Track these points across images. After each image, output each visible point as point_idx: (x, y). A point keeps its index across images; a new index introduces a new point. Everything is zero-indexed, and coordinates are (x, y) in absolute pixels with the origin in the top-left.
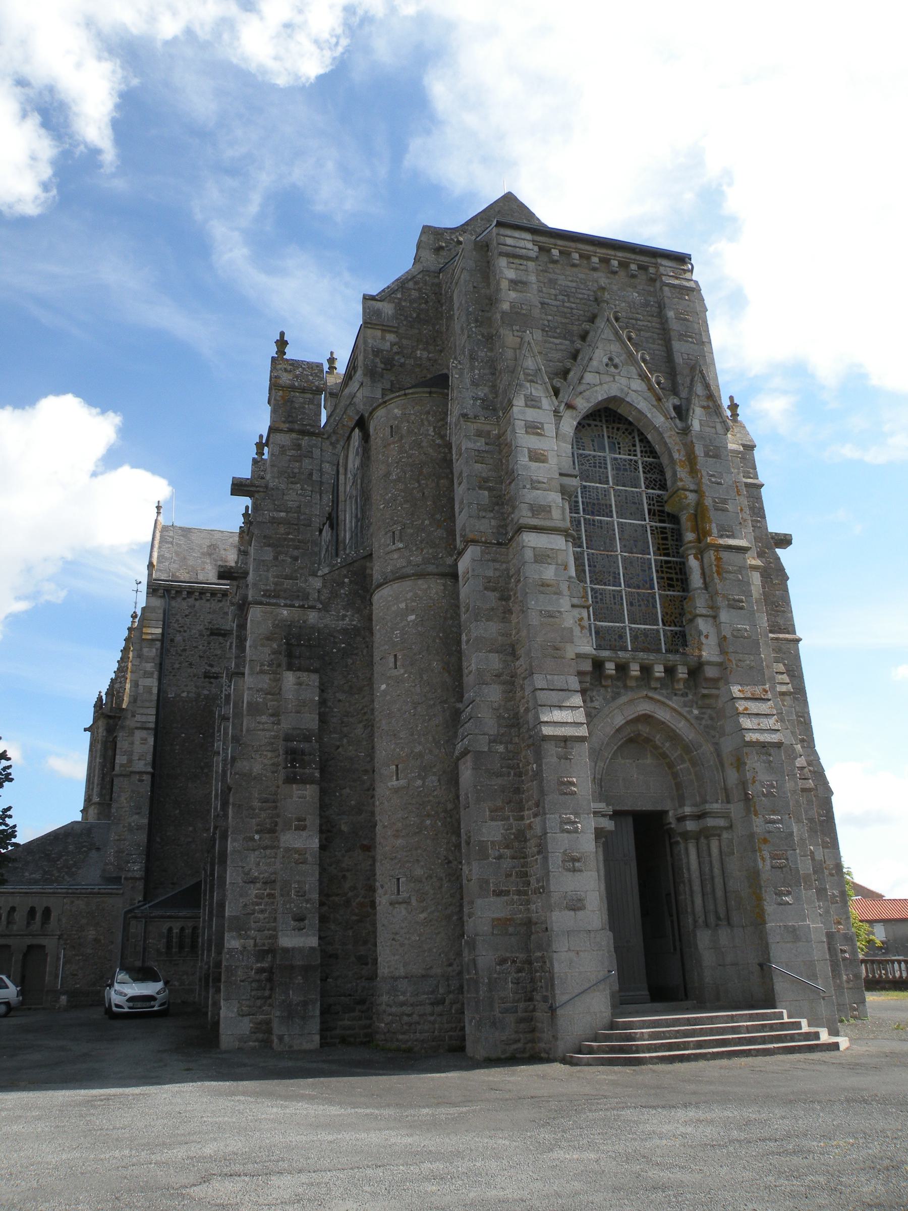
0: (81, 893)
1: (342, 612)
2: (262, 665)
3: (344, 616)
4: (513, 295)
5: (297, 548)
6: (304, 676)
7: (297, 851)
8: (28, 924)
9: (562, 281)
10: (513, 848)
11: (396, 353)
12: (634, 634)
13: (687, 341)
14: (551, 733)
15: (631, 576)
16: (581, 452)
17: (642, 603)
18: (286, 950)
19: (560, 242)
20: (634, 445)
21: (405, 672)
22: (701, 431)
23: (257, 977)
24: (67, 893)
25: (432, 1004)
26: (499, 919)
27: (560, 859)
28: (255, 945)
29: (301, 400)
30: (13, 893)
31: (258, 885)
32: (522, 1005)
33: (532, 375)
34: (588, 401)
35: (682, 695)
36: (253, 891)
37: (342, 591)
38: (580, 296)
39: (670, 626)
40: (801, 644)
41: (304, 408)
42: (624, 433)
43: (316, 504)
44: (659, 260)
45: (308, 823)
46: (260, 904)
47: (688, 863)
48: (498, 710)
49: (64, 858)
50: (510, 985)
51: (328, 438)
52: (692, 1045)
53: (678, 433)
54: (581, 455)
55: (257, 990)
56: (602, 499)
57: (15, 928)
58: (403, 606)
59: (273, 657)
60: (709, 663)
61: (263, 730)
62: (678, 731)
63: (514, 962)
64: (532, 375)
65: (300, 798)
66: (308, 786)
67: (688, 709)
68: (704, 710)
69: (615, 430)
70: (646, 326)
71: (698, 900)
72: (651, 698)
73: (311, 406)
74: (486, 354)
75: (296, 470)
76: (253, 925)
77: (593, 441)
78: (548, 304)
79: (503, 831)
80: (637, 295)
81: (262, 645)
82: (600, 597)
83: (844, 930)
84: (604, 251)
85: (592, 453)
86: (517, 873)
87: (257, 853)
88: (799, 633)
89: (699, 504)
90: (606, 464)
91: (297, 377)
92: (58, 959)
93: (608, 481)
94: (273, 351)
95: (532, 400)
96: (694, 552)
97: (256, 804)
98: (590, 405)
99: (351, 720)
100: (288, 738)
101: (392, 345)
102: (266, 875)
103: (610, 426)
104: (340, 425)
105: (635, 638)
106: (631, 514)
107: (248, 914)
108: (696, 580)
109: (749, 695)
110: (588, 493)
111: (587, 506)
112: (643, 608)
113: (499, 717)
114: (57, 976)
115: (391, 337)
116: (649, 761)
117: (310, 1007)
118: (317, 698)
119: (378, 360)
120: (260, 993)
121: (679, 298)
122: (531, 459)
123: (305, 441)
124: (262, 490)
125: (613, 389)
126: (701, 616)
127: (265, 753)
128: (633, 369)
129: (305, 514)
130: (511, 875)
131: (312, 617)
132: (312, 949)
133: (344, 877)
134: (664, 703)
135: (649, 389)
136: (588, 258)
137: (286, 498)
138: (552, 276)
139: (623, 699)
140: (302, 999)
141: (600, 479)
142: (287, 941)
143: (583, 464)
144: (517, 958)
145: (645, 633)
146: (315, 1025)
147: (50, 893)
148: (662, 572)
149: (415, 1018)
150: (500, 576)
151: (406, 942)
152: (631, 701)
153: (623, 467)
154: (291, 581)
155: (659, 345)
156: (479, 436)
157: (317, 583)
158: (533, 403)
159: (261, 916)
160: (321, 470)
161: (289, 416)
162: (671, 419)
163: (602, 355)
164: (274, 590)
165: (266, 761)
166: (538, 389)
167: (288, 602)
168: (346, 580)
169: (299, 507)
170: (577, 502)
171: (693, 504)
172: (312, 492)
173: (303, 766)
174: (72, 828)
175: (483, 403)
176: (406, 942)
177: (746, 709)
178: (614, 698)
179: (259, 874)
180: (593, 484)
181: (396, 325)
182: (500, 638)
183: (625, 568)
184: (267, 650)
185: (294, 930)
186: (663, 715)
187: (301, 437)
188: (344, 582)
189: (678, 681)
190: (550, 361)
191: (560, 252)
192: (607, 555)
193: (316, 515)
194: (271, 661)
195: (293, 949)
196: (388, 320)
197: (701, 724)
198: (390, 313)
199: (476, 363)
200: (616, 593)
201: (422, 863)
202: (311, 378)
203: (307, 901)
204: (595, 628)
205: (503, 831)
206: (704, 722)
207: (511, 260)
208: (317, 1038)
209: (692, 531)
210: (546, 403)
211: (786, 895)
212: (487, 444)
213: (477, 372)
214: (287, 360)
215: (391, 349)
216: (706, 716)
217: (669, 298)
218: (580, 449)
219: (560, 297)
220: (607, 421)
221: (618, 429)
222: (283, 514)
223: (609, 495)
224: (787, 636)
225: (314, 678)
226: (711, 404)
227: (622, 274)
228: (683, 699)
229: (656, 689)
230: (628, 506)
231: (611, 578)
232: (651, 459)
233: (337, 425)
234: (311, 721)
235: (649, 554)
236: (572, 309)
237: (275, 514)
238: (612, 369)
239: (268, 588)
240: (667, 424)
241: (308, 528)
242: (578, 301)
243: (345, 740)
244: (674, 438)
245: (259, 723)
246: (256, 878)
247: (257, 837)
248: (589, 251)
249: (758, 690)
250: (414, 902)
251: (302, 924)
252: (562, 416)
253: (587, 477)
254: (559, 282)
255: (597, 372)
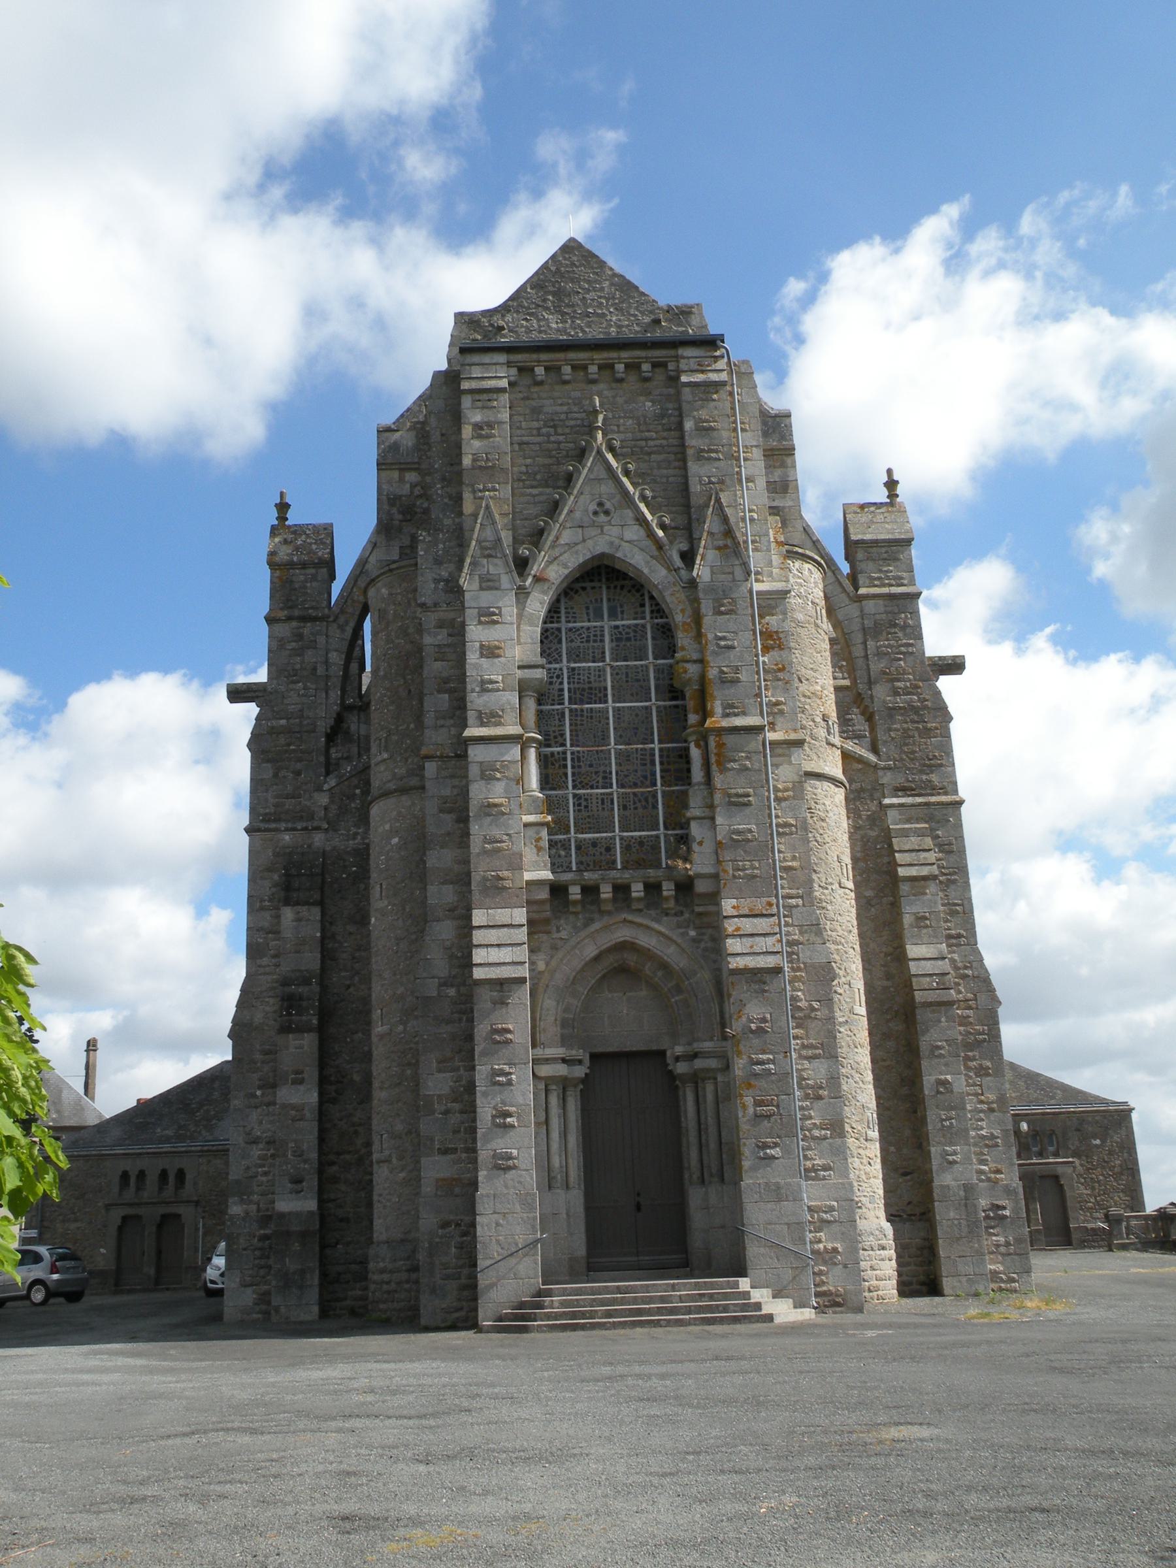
0: (218, 1151)
1: (353, 830)
2: (262, 901)
3: (356, 834)
4: (477, 443)
5: (300, 760)
6: (304, 911)
7: (294, 1107)
8: (161, 1189)
9: (549, 408)
10: (462, 1101)
11: (420, 496)
12: (625, 843)
13: (710, 459)
14: (483, 977)
15: (626, 773)
16: (571, 625)
17: (638, 805)
18: (282, 1215)
19: (544, 356)
20: (643, 605)
21: (389, 904)
22: (712, 581)
23: (260, 1244)
24: (202, 1151)
25: (408, 1271)
26: (443, 1180)
27: (489, 1115)
28: (258, 1210)
29: (302, 578)
30: (141, 1154)
31: (261, 1146)
32: (465, 1271)
33: (490, 549)
34: (565, 566)
35: (676, 915)
36: (256, 1152)
37: (353, 805)
38: (572, 423)
39: (674, 829)
40: (963, 808)
41: (305, 587)
42: (629, 591)
43: (321, 704)
44: (681, 351)
45: (305, 1075)
46: (264, 1166)
47: (686, 1111)
48: (450, 948)
49: (205, 1108)
50: (453, 1249)
51: (334, 621)
52: (600, 1313)
53: (684, 587)
54: (570, 630)
55: (260, 1258)
56: (595, 681)
57: (146, 1194)
58: (387, 827)
59: (274, 890)
60: (699, 876)
61: (265, 974)
62: (665, 958)
63: (458, 1225)
64: (490, 549)
65: (296, 1048)
66: (306, 1035)
67: (681, 930)
68: (704, 931)
69: (618, 590)
70: (661, 446)
71: (694, 1154)
72: (631, 922)
73: (315, 584)
74: (454, 521)
75: (298, 666)
76: (256, 1189)
77: (587, 608)
78: (527, 443)
79: (452, 1084)
80: (650, 404)
81: (262, 878)
82: (584, 803)
83: (1006, 1179)
84: (605, 355)
85: (586, 624)
86: (465, 1129)
87: (259, 1110)
88: (963, 792)
89: (703, 679)
90: (603, 635)
91: (297, 549)
92: (197, 1229)
93: (604, 657)
94: (272, 517)
95: (489, 580)
96: (694, 738)
97: (258, 1056)
98: (566, 572)
99: (363, 954)
100: (285, 982)
101: (413, 486)
102: (269, 1134)
103: (612, 586)
104: (349, 601)
105: (627, 848)
106: (632, 695)
107: (251, 1177)
108: (697, 774)
109: (746, 912)
110: (576, 677)
111: (575, 693)
112: (640, 810)
113: (452, 957)
114: (196, 1250)
115: (411, 477)
116: (644, 993)
117: (308, 1276)
118: (318, 934)
119: (394, 510)
120: (263, 1262)
121: (703, 400)
122: (482, 655)
123: (307, 629)
124: (260, 694)
125: (598, 545)
126: (695, 818)
127: (267, 1000)
128: (629, 513)
129: (309, 718)
130: (459, 1131)
131: (318, 839)
132: (311, 1213)
133: (356, 1132)
134: (648, 927)
135: (648, 536)
136: (585, 368)
137: (286, 701)
138: (534, 403)
139: (596, 926)
140: (300, 1267)
141: (594, 657)
142: (284, 1205)
143: (572, 641)
144: (461, 1220)
145: (641, 842)
146: (313, 1295)
147: (182, 1152)
148: (669, 763)
149: (393, 1286)
150: (458, 795)
151: (388, 1204)
152: (605, 928)
153: (625, 636)
154: (293, 800)
155: (675, 468)
156: (440, 627)
157: (324, 799)
158: (489, 584)
159: (264, 1179)
160: (326, 662)
161: (288, 600)
162: (675, 570)
163: (588, 501)
164: (275, 813)
165: (268, 1009)
166: (496, 565)
167: (290, 825)
168: (358, 791)
169: (301, 710)
170: (562, 690)
171: (696, 678)
172: (316, 690)
173: (299, 1014)
174: (222, 1071)
175: (446, 585)
176: (388, 1204)
177: (738, 929)
178: (586, 925)
179: (262, 1133)
180: (584, 664)
181: (416, 460)
182: (456, 866)
183: (618, 764)
184: (267, 883)
185: (291, 1193)
186: (646, 940)
187: (302, 624)
188: (355, 794)
189: (667, 898)
190: (526, 519)
191: (547, 369)
192: (597, 751)
193: (321, 717)
194: (273, 894)
195: (290, 1213)
196: (407, 455)
197: (698, 948)
198: (410, 444)
199: (441, 536)
200: (605, 797)
201: (402, 1118)
202: (314, 547)
203: (305, 1161)
204: (576, 841)
205: (452, 1084)
206: (703, 945)
207: (477, 397)
208: (316, 1309)
209: (696, 712)
210: (505, 581)
211: (770, 1147)
212: (450, 635)
213: (441, 546)
214: (289, 527)
215: (412, 492)
216: (706, 937)
217: (689, 402)
218: (569, 622)
219: (544, 430)
220: (608, 579)
221: (622, 587)
222: (283, 722)
223: (605, 675)
224: (944, 798)
225: (316, 912)
226: (729, 542)
227: (632, 378)
228: (675, 919)
229: (640, 910)
230: (630, 685)
231: (600, 779)
232: (660, 620)
233: (346, 601)
234: (311, 960)
235: (653, 742)
236: (560, 443)
237: (274, 723)
238: (602, 518)
239: (267, 811)
240: (671, 579)
241: (312, 735)
242: (567, 430)
243: (357, 978)
244: (678, 595)
245: (259, 966)
246: (258, 1138)
247: (259, 1093)
248: (584, 360)
249: (759, 905)
250: (394, 1160)
251: (298, 1187)
252: (529, 593)
253: (577, 656)
254: (546, 409)
255: (579, 527)
